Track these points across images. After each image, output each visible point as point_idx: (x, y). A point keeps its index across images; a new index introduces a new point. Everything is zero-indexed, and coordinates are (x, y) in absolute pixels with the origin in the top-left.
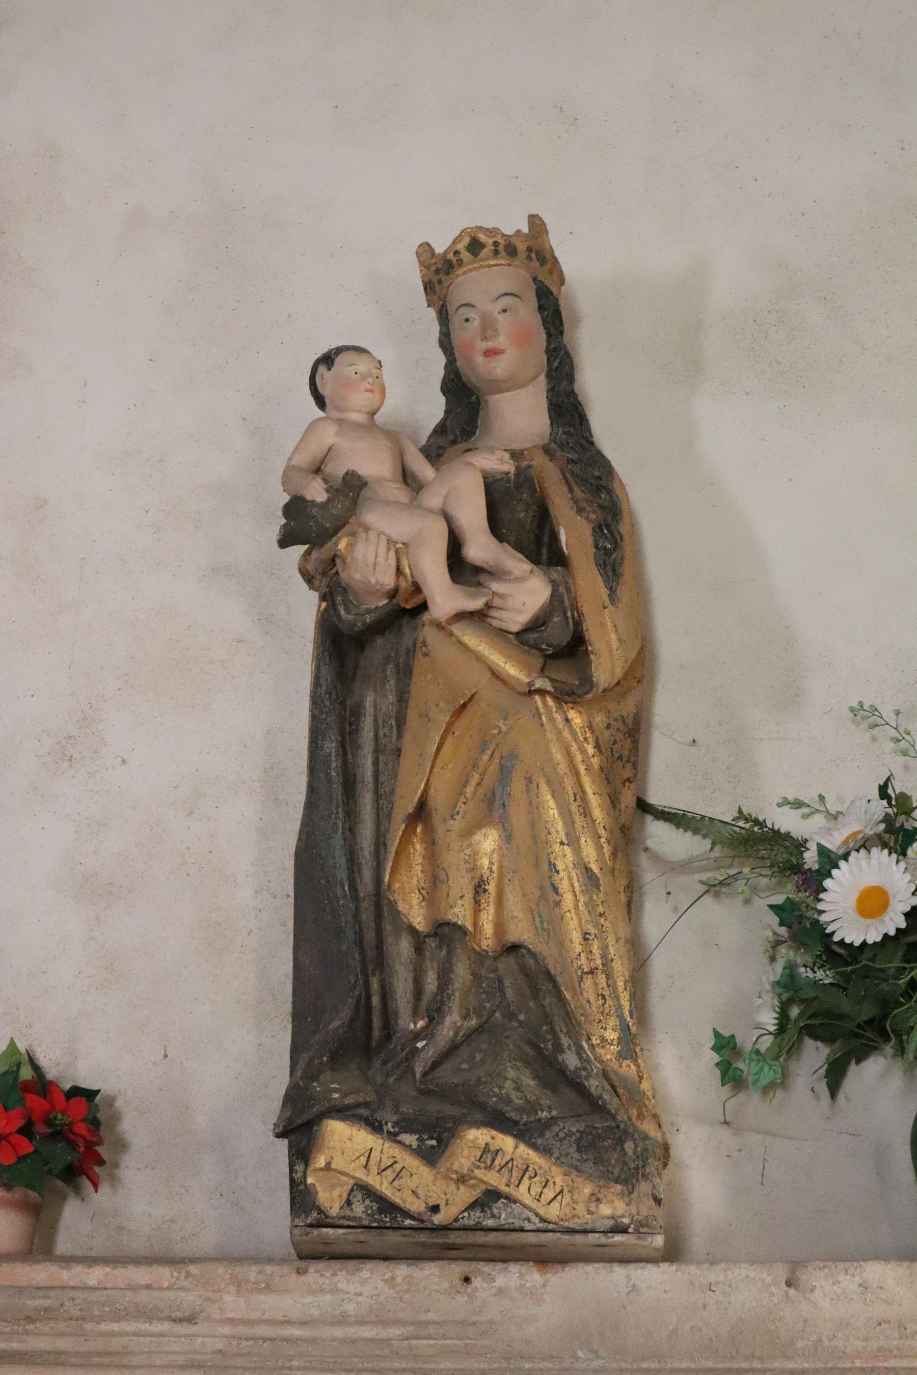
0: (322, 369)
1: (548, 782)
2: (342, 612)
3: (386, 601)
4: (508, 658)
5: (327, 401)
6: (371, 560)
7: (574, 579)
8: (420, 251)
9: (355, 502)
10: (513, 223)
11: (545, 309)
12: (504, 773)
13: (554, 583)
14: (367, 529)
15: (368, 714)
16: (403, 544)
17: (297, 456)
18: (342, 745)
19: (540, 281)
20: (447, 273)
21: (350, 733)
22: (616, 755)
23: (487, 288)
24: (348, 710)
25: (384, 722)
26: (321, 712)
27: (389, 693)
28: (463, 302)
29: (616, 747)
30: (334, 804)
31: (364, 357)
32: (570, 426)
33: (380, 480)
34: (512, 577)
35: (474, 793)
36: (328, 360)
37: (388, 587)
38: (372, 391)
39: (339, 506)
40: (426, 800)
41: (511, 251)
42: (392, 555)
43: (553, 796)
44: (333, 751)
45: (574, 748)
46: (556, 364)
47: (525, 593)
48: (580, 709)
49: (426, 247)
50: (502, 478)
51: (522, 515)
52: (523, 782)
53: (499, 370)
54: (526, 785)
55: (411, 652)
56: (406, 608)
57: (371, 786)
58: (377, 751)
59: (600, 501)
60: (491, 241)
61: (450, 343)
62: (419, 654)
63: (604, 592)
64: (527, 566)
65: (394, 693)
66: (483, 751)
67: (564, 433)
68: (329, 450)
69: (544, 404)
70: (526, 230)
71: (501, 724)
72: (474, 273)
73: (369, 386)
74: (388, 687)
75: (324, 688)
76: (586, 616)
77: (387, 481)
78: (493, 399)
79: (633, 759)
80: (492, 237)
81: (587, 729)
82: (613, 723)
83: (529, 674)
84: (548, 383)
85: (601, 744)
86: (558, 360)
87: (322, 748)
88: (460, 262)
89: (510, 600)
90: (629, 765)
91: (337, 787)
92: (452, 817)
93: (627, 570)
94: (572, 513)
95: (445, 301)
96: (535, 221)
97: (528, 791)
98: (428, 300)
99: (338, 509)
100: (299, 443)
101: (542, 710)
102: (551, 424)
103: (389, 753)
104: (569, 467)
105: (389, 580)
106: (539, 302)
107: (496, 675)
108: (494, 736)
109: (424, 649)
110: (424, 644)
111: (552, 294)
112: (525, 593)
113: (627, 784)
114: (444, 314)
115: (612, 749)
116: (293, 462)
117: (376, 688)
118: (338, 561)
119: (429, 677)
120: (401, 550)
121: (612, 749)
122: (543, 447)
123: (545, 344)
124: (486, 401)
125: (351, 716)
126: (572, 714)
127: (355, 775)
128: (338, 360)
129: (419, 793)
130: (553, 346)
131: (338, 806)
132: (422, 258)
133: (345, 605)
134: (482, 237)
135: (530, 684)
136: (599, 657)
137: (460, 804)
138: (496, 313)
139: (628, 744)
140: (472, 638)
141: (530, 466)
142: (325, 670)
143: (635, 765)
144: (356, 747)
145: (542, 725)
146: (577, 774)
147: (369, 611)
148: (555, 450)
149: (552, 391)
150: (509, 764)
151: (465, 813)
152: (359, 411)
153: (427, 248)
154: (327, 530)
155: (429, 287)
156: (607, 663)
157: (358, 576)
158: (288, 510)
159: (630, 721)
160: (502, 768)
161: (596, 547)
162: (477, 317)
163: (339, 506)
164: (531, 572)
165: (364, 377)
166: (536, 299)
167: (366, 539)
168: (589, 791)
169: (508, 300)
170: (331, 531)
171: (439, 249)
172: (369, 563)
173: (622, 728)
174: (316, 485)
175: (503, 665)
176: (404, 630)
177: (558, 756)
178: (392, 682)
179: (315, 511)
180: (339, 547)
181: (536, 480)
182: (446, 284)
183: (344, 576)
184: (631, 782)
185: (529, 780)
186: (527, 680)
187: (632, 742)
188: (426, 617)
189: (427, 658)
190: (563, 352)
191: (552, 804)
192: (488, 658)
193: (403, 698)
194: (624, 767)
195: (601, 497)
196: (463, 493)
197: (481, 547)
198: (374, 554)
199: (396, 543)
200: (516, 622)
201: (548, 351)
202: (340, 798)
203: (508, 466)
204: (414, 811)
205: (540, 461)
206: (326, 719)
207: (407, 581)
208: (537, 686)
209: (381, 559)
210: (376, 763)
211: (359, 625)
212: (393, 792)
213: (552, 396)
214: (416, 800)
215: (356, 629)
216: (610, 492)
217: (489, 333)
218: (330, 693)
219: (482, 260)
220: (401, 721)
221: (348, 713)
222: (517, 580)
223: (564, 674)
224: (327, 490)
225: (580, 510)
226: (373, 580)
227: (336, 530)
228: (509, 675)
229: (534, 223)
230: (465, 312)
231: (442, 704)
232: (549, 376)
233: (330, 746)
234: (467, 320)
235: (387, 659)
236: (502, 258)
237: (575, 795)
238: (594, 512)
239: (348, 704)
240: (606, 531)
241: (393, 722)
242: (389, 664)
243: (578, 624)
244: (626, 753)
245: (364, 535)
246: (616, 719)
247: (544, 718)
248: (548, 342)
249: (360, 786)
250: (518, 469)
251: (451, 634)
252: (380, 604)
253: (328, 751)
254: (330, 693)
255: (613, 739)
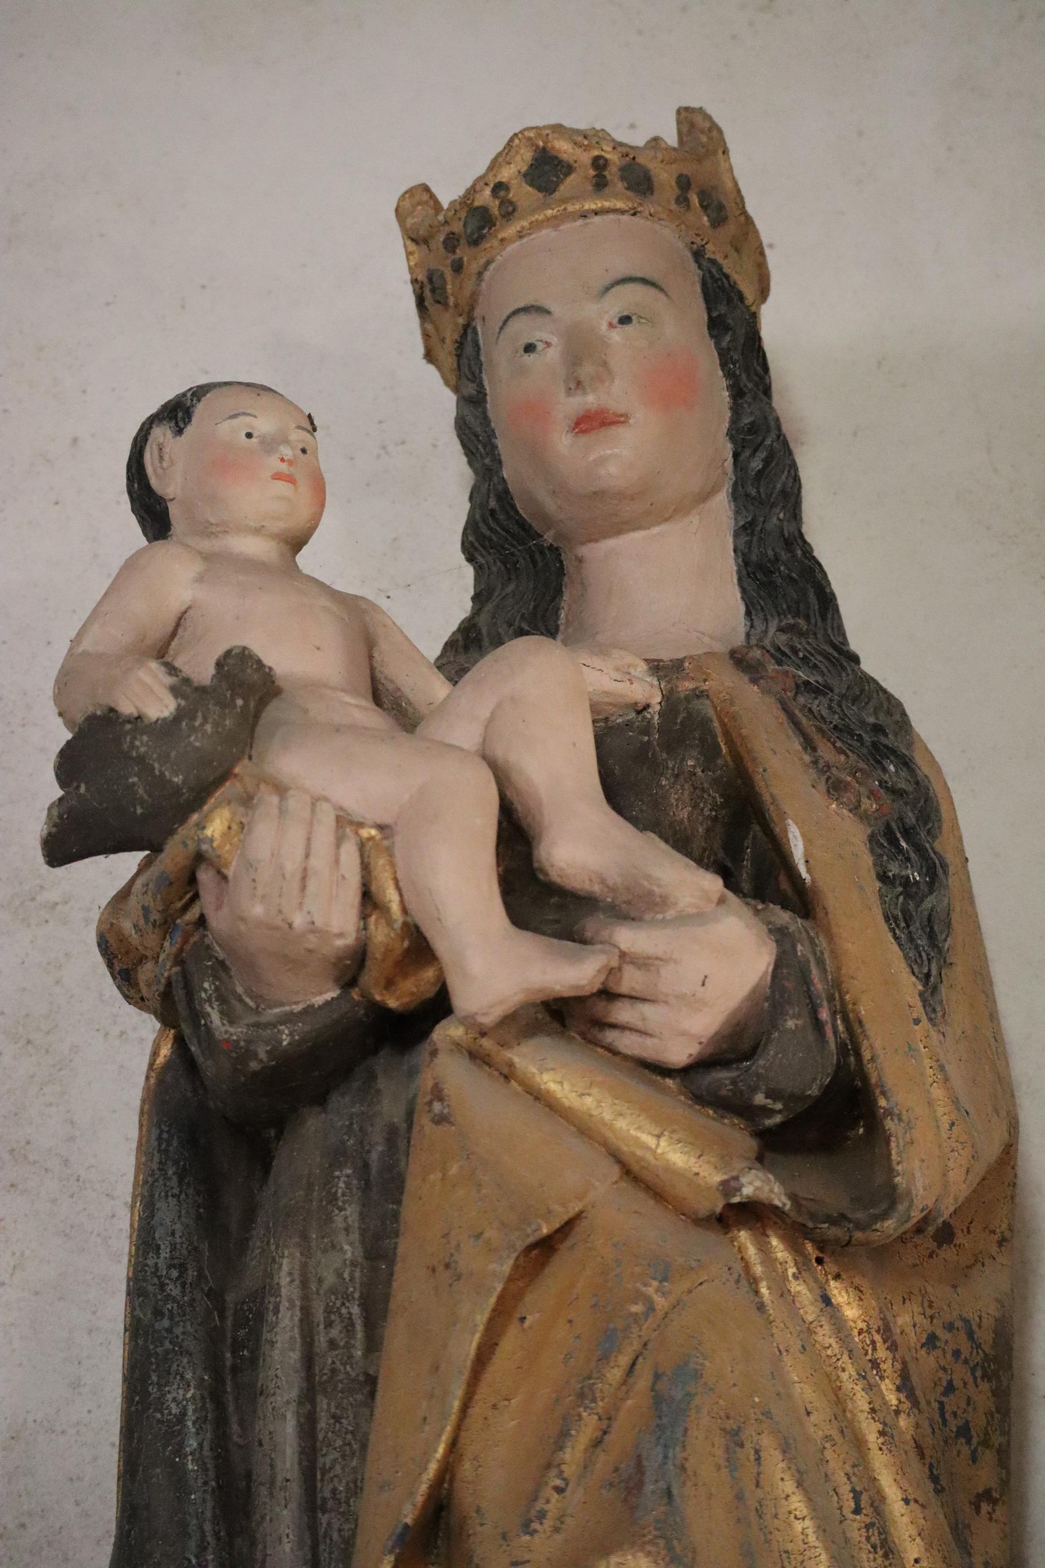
0: (161, 433)
1: (785, 1448)
2: (215, 1017)
3: (329, 996)
4: (663, 1124)
5: (174, 511)
6: (292, 865)
7: (830, 938)
8: (407, 204)
9: (251, 721)
10: (643, 121)
11: (727, 328)
12: (667, 1414)
13: (780, 934)
14: (281, 790)
15: (285, 1304)
16: (381, 827)
17: (95, 629)
18: (215, 1395)
19: (713, 262)
20: (475, 242)
21: (235, 1370)
22: (953, 1424)
23: (571, 270)
24: (230, 1313)
25: (328, 1311)
26: (158, 1313)
27: (342, 1237)
28: (521, 304)
29: (952, 1403)
30: (192, 1544)
31: (266, 399)
32: (797, 614)
33: (314, 687)
34: (670, 914)
35: (586, 1466)
36: (177, 413)
37: (340, 943)
38: (290, 479)
39: (208, 728)
40: (450, 1491)
41: (639, 181)
42: (350, 855)
43: (799, 1484)
44: (191, 1408)
45: (848, 1376)
46: (756, 464)
47: (703, 962)
48: (857, 1280)
49: (421, 195)
50: (628, 724)
51: (684, 814)
52: (719, 1441)
53: (613, 469)
54: (727, 1450)
55: (399, 1138)
56: (388, 1016)
57: (295, 1488)
58: (309, 1395)
59: (886, 777)
60: (585, 158)
61: (486, 420)
62: (424, 1121)
63: (910, 987)
64: (713, 883)
65: (355, 1236)
66: (605, 1358)
67: (781, 630)
68: (178, 625)
69: (728, 565)
70: (671, 139)
71: (650, 1291)
72: (546, 233)
73: (284, 467)
74: (339, 1221)
75: (165, 1253)
76: (867, 1026)
77: (334, 689)
78: (595, 552)
79: (997, 1439)
80: (587, 148)
81: (877, 1338)
82: (943, 1335)
83: (725, 1160)
84: (737, 512)
85: (915, 1379)
86: (762, 454)
87: (160, 1401)
88: (509, 211)
89: (667, 972)
90: (988, 1457)
91: (201, 1501)
92: (526, 1527)
93: (955, 942)
94: (818, 796)
95: (471, 319)
96: (694, 123)
97: (732, 1464)
98: (426, 336)
99: (201, 737)
100: (100, 603)
101: (758, 1270)
102: (748, 613)
103: (346, 1391)
104: (801, 700)
105: (338, 919)
106: (709, 310)
107: (633, 1174)
108: (635, 1318)
109: (437, 1107)
110: (438, 1093)
111: (741, 298)
112: (703, 962)
113: (985, 1507)
114: (469, 349)
115: (942, 1404)
116: (87, 645)
117: (304, 1237)
118: (205, 876)
119: (454, 1170)
120: (375, 847)
121: (942, 1404)
122: (733, 653)
123: (728, 414)
124: (580, 560)
125: (237, 1326)
126: (839, 1293)
127: (248, 1475)
128: (200, 410)
129: (433, 1467)
130: (746, 420)
131: (203, 1548)
132: (410, 221)
133: (222, 999)
134: (563, 147)
135: (728, 1187)
136: (909, 1127)
137: (548, 1492)
138: (604, 327)
139: (982, 1395)
140: (559, 1074)
141: (699, 694)
142: (167, 1212)
143: (1003, 1456)
144: (252, 1395)
145: (761, 1307)
146: (859, 1443)
147: (288, 1019)
148: (760, 663)
149: (747, 531)
150: (678, 1395)
151: (561, 1519)
152: (258, 531)
153: (425, 197)
154: (177, 790)
155: (429, 295)
156: (926, 1161)
157: (258, 910)
158: (70, 765)
159: (985, 1336)
160: (658, 1400)
161: (883, 877)
162: (554, 340)
163: (208, 728)
164: (722, 901)
165: (270, 445)
166: (703, 305)
167: (282, 812)
168: (892, 1492)
169: (630, 297)
170: (186, 795)
171: (447, 195)
172: (287, 872)
173: (965, 1353)
174: (148, 679)
175: (651, 1142)
176: (381, 1083)
177: (805, 1392)
178: (352, 1212)
179: (142, 744)
180: (209, 832)
181: (716, 724)
182: (474, 267)
183: (218, 921)
184: (994, 1502)
185: (735, 1438)
186: (717, 1178)
187: (995, 1393)
188: (448, 1032)
189: (446, 1127)
190: (773, 435)
191: (797, 1503)
192: (611, 1127)
193: (379, 1252)
194: (974, 1460)
195: (885, 770)
196: (547, 714)
197: (584, 842)
198: (300, 852)
199: (361, 825)
200: (683, 1033)
201: (733, 434)
202: (208, 1527)
203: (646, 691)
204: (416, 1521)
205: (725, 681)
206: (169, 1330)
207: (390, 923)
208: (748, 1191)
209: (320, 862)
210: (308, 1427)
211: (262, 1056)
212: (356, 1489)
213: (749, 544)
214: (424, 1488)
215: (254, 1065)
216: (906, 763)
217: (587, 370)
218: (182, 1268)
219: (564, 201)
220: (375, 1307)
221: (229, 1322)
222: (684, 919)
223: (821, 1186)
224: (175, 691)
225: (835, 788)
226: (299, 921)
227: (199, 796)
228: (669, 1169)
229: (692, 125)
230: (524, 329)
231: (490, 1233)
232: (737, 495)
233: (183, 1395)
234: (529, 348)
235: (337, 1156)
236: (616, 196)
237: (857, 1495)
238: (872, 794)
239: (230, 1298)
240: (904, 844)
241: (356, 1310)
242: (341, 1167)
243: (851, 1047)
244: (978, 1421)
245: (275, 799)
246: (950, 1327)
247: (764, 1290)
248: (736, 411)
249: (264, 1491)
250: (670, 700)
251: (508, 1075)
252: (319, 1000)
253: (175, 1410)
254: (182, 1268)
255: (945, 1378)
